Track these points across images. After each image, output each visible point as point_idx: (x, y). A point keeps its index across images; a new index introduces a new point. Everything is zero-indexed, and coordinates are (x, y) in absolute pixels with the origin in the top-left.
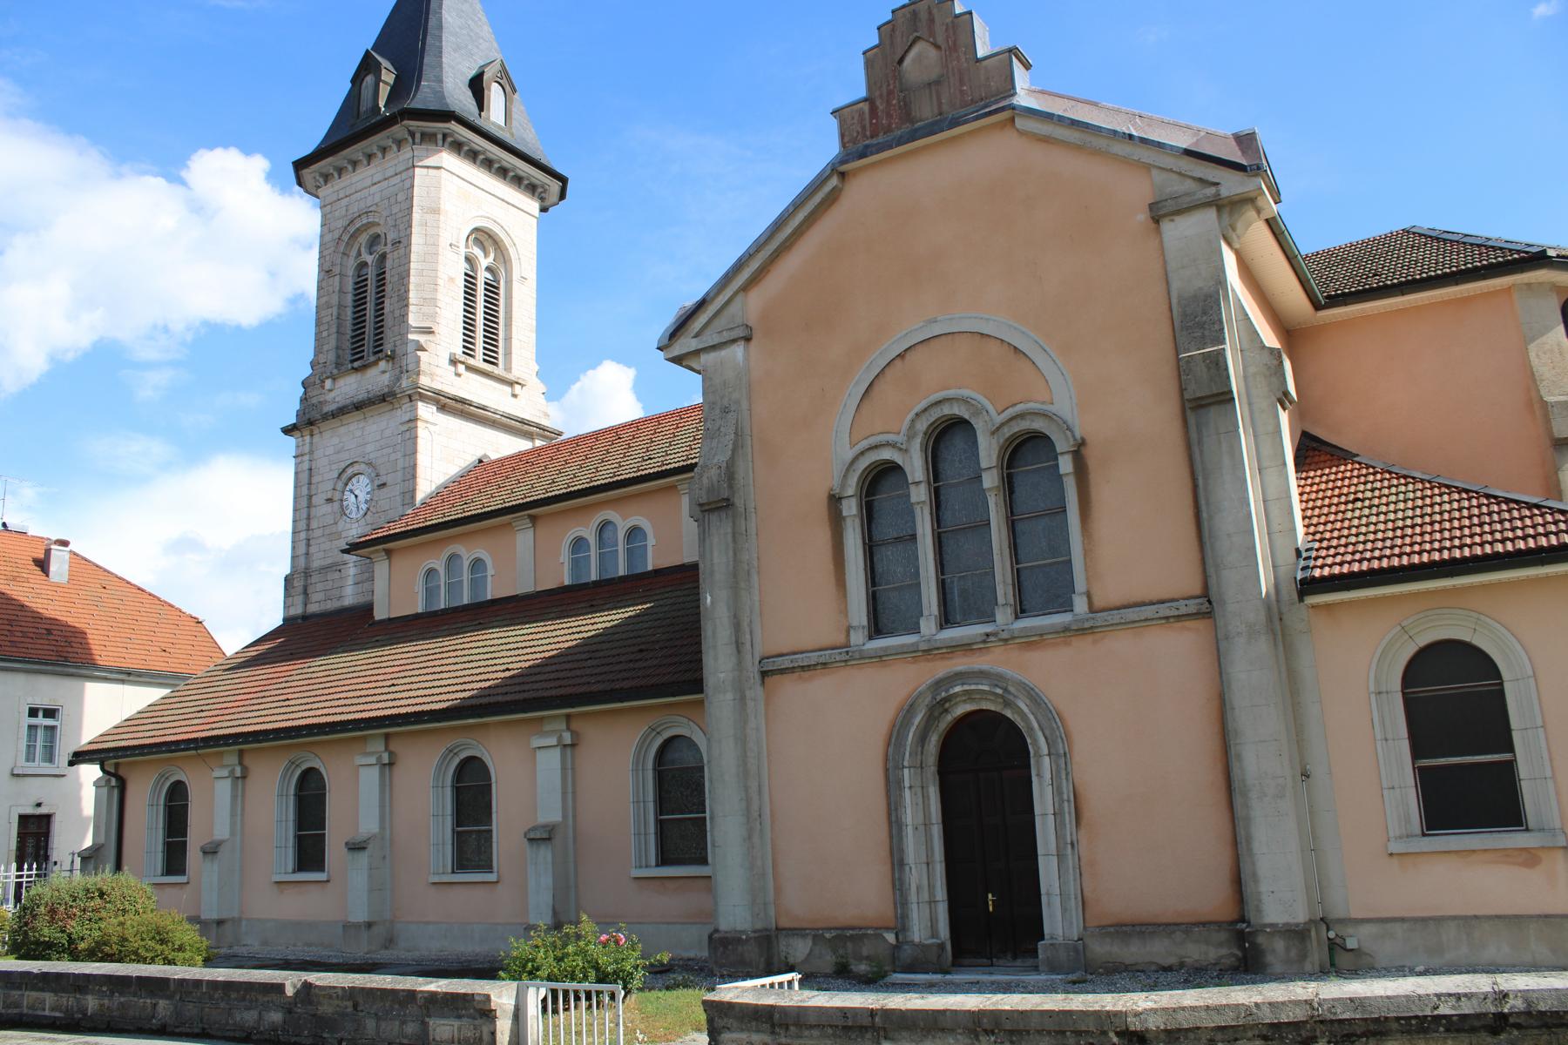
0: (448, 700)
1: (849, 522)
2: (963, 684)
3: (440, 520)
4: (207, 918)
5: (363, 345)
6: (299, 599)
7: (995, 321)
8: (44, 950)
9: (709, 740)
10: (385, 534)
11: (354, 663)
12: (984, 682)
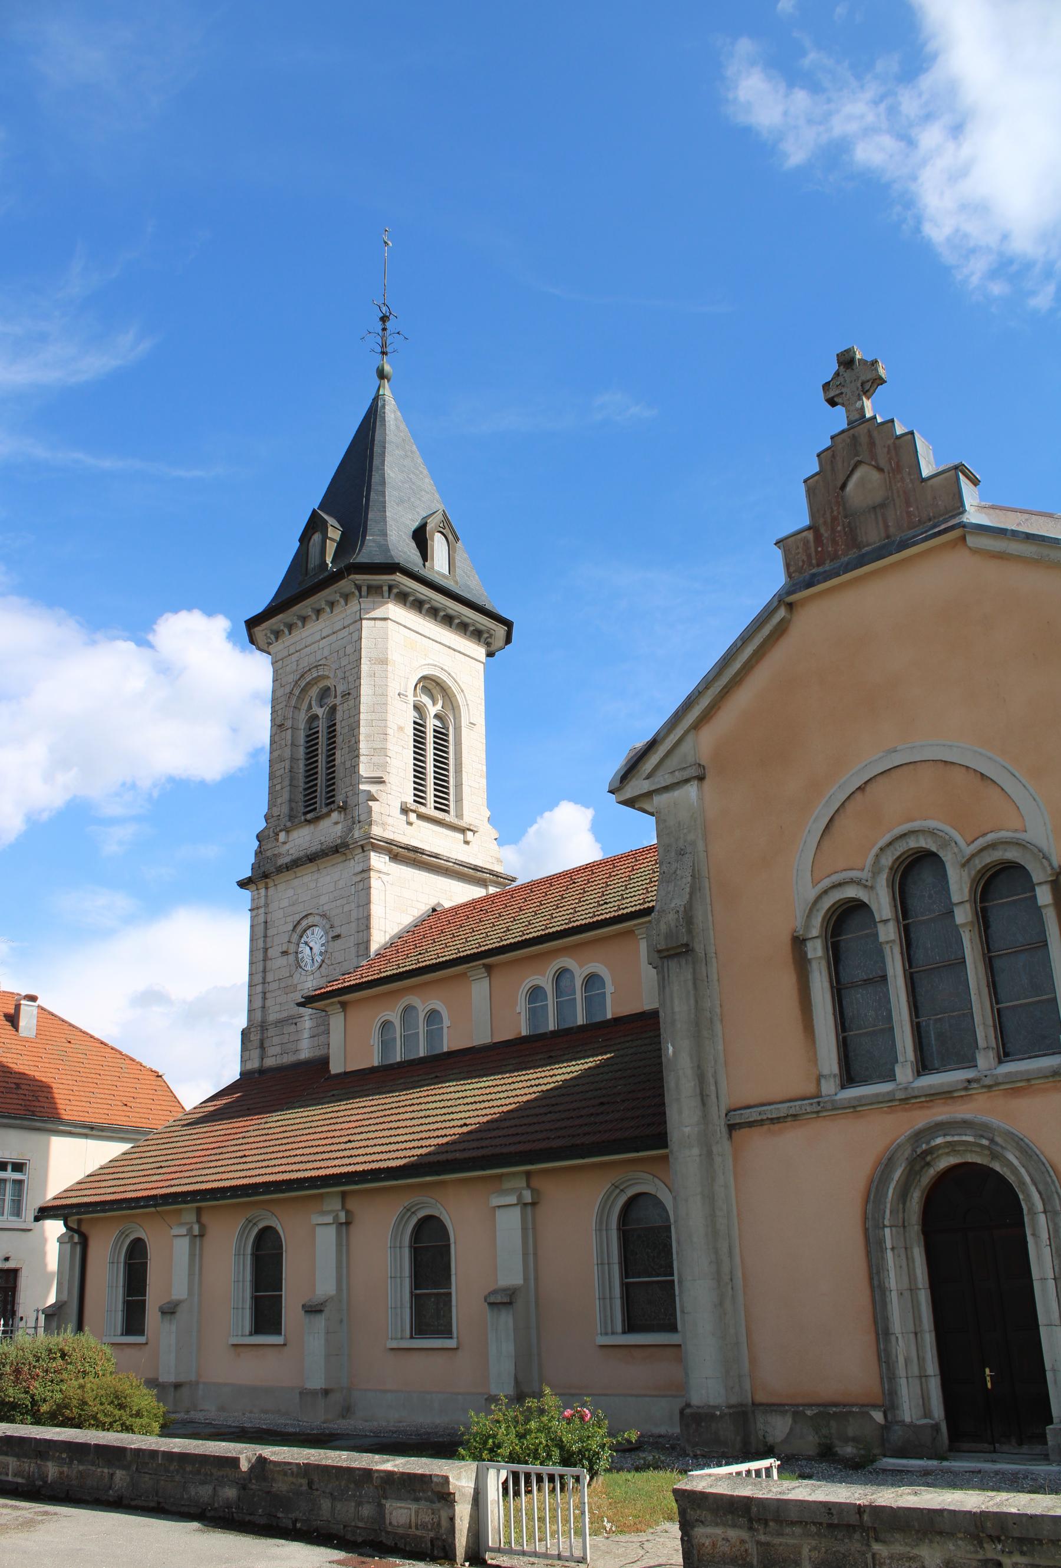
0: (405, 1157)
1: (815, 965)
2: (945, 1135)
3: (395, 972)
4: (166, 1380)
5: (316, 797)
6: (255, 1054)
7: (958, 747)
8: (9, 1411)
9: (675, 1198)
10: (340, 986)
11: (310, 1119)
12: (968, 1132)
